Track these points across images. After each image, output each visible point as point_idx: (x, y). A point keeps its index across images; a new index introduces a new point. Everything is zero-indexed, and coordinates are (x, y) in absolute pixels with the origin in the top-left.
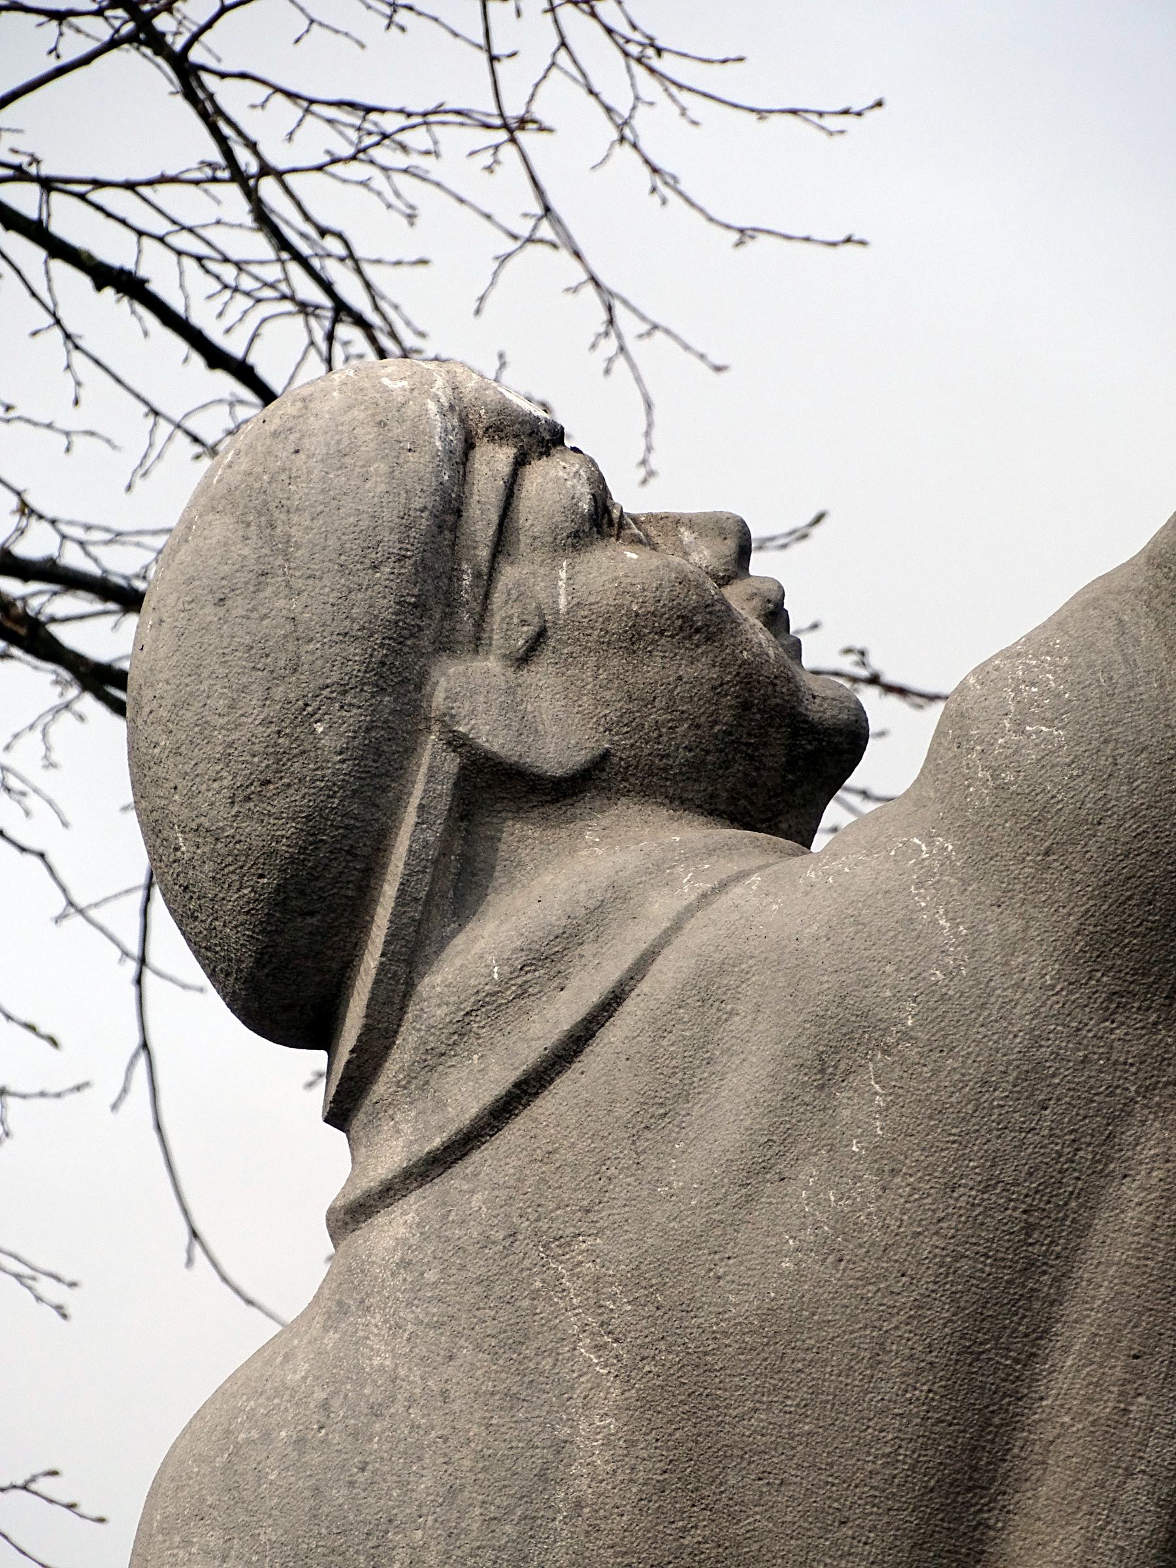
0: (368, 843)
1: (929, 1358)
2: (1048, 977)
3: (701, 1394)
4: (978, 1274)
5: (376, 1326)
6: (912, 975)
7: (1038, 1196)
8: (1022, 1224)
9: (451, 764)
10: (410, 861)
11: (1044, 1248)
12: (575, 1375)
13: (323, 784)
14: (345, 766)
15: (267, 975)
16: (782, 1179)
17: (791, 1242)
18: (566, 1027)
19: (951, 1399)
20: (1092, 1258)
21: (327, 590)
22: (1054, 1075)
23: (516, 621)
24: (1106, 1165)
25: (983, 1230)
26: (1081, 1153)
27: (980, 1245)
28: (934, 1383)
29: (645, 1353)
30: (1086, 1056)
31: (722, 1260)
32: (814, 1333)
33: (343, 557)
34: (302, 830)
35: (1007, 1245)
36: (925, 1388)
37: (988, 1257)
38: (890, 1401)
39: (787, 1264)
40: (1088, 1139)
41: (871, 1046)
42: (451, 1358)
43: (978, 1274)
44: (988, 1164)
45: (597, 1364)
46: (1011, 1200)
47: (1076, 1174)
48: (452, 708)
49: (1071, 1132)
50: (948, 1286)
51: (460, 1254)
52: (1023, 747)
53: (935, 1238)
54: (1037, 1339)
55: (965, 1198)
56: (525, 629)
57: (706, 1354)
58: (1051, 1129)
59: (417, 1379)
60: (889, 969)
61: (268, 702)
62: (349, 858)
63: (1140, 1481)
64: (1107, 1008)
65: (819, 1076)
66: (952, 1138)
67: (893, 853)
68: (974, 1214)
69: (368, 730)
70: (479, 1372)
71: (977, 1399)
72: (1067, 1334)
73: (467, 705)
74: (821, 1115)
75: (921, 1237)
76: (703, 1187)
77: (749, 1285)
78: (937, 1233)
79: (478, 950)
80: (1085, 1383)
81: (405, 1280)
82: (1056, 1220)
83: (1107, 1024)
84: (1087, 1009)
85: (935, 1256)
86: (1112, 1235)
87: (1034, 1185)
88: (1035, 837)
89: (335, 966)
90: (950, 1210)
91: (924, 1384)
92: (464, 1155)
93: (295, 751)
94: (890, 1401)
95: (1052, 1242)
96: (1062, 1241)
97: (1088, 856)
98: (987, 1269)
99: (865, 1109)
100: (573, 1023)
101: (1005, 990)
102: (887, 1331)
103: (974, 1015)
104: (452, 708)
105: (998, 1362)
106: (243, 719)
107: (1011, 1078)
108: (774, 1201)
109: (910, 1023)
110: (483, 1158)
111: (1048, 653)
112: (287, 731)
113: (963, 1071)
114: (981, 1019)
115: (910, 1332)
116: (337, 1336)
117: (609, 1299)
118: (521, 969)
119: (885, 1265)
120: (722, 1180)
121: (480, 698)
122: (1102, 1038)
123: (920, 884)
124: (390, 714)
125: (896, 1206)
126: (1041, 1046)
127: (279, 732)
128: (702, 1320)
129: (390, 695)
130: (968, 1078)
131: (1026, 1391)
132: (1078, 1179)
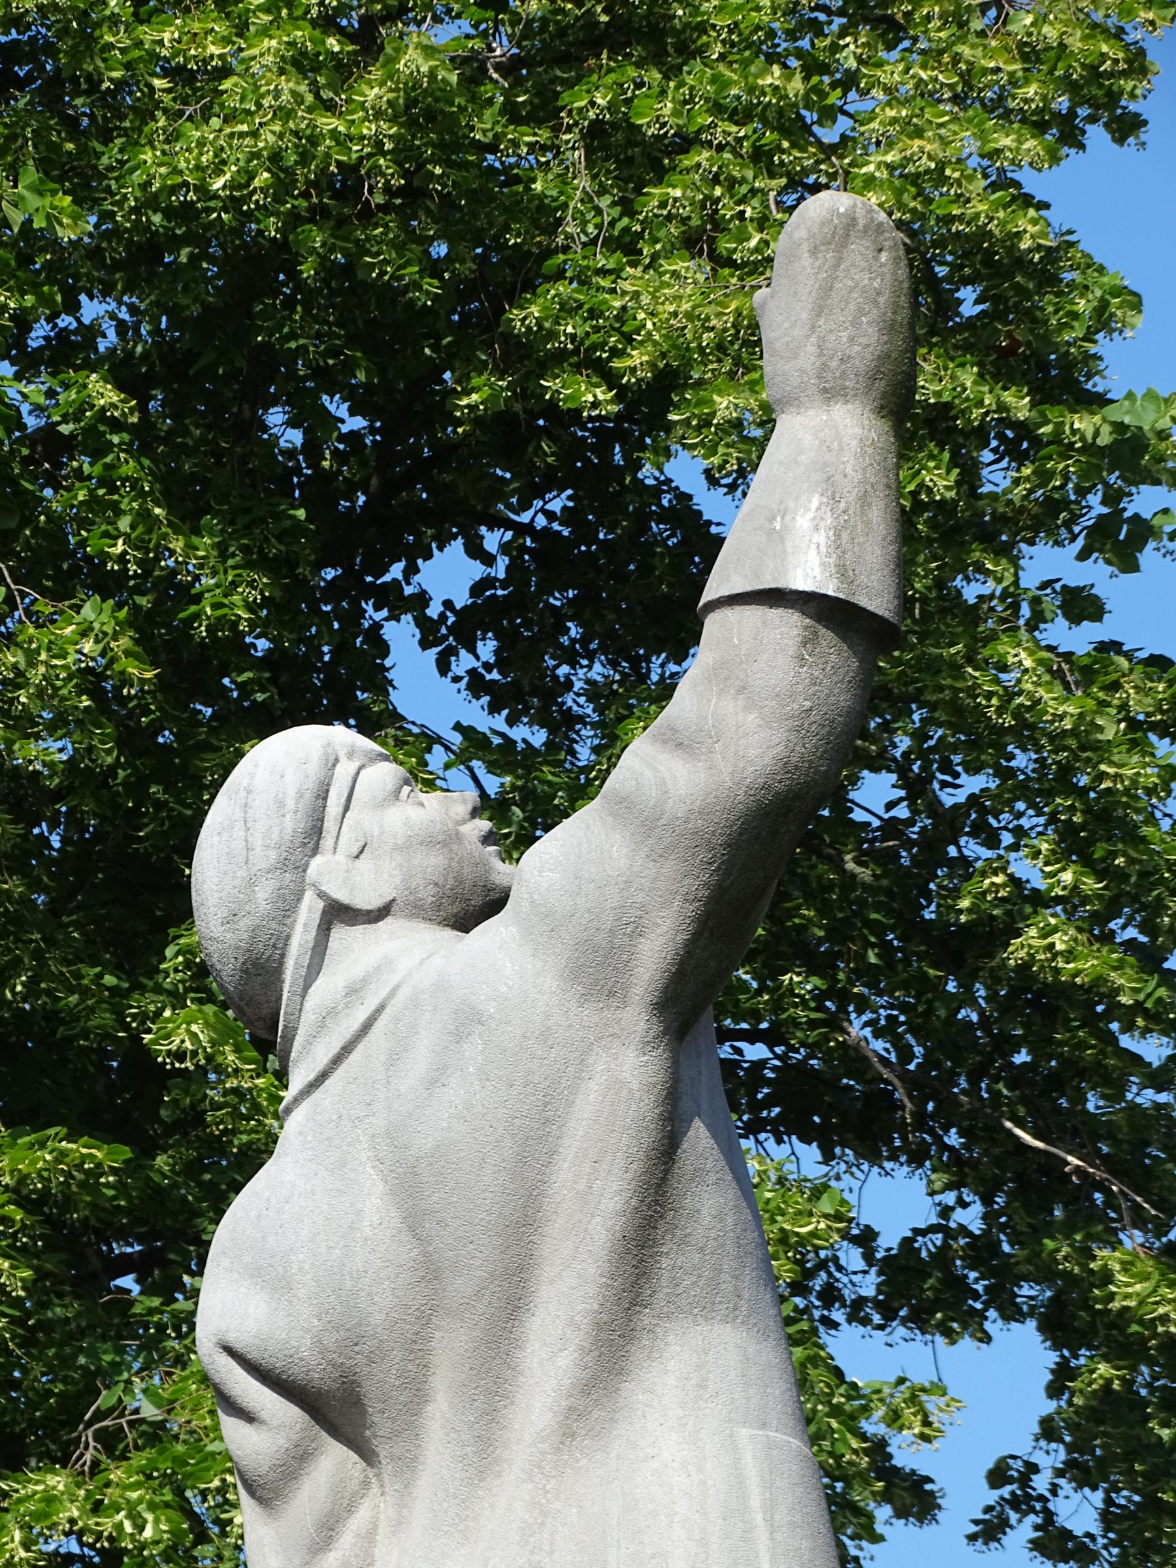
9: (320, 905)
63: (598, 1219)
99: (473, 1050)
121: (332, 873)
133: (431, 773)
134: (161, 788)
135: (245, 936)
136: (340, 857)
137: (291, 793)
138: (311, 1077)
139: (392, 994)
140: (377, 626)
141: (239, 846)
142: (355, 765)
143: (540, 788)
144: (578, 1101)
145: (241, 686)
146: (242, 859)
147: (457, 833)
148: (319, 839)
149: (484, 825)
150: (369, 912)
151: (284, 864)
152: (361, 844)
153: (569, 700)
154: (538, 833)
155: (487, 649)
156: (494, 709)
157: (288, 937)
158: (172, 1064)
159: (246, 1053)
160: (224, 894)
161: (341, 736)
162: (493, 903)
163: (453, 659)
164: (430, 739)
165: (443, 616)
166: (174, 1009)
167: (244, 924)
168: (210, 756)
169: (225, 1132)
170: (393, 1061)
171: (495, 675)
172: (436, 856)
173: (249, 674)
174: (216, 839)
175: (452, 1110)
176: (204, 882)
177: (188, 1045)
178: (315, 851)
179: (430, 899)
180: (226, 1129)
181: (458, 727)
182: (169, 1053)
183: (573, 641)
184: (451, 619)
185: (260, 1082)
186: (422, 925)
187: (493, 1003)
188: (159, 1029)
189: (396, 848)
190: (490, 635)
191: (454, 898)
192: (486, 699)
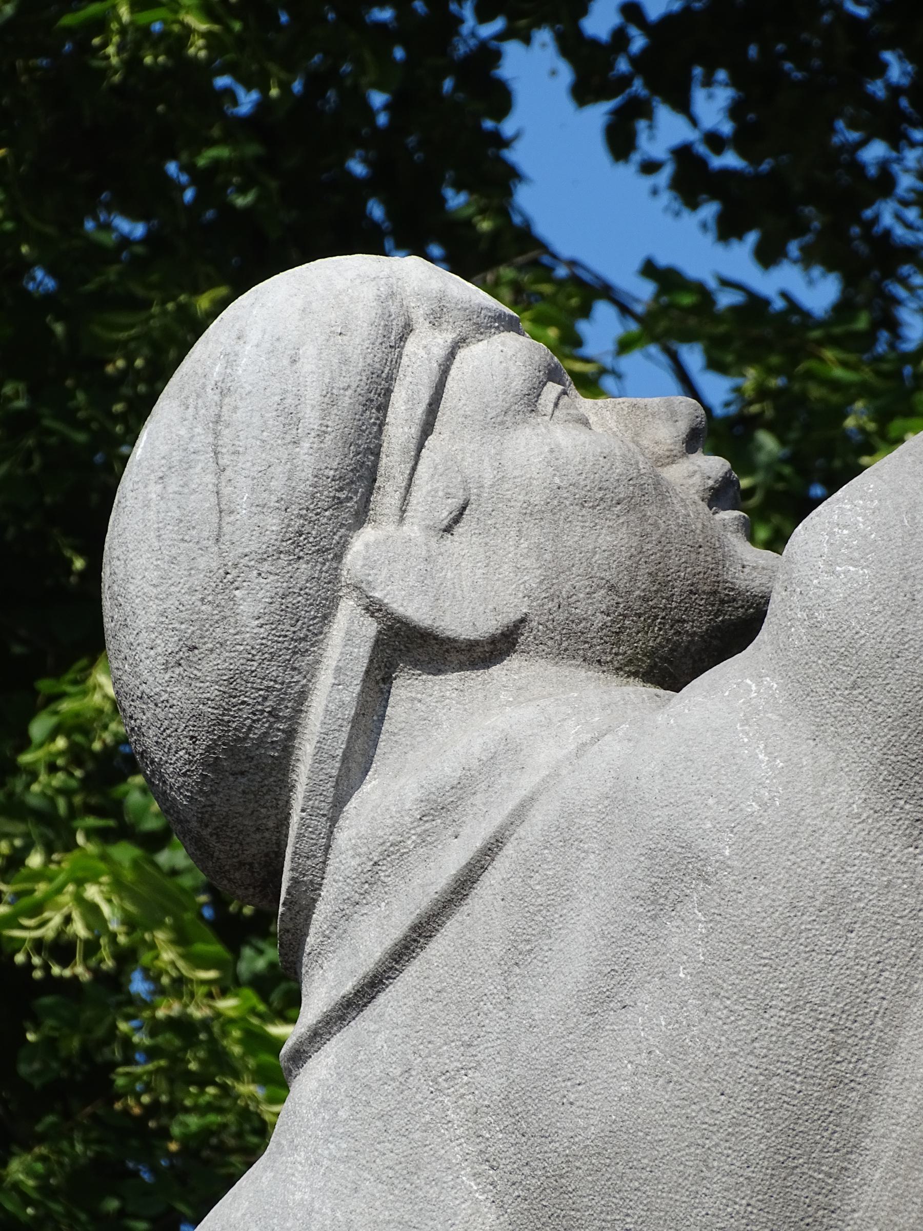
0: (290, 705)
1: (748, 1173)
2: (855, 806)
3: (558, 1216)
4: (789, 1091)
5: (301, 1164)
6: (731, 807)
7: (844, 1016)
8: (830, 1043)
9: (370, 628)
10: (327, 721)
11: (851, 1066)
12: (457, 1202)
13: (242, 648)
14: (262, 630)
15: (211, 835)
16: (624, 1007)
17: (629, 1066)
18: (454, 872)
19: (768, 1212)
20: (898, 1075)
21: (249, 464)
22: (859, 900)
23: (441, 494)
24: (910, 985)
25: (792, 1049)
26: (886, 974)
27: (790, 1063)
28: (752, 1198)
29: (514, 1178)
30: (889, 881)
31: (573, 1086)
32: (648, 1153)
33: (265, 434)
34: (224, 692)
35: (816, 1063)
36: (744, 1202)
37: (798, 1075)
38: (713, 1215)
39: (626, 1088)
40: (893, 961)
41: (694, 876)
42: (356, 1190)
43: (789, 1091)
44: (796, 986)
45: (476, 1191)
46: (819, 1020)
47: (881, 994)
48: (369, 575)
49: (876, 954)
50: (761, 1104)
51: (366, 1091)
52: (833, 586)
53: (750, 1057)
54: (848, 1153)
55: (776, 1018)
56: (450, 501)
57: (561, 1176)
58: (856, 952)
59: (329, 1212)
60: (711, 801)
61: (193, 572)
62: (272, 720)
64: (911, 835)
65: (651, 908)
66: (763, 961)
67: (727, 694)
68: (784, 1034)
69: (284, 597)
70: (378, 1203)
71: (792, 1212)
72: (875, 1148)
73: (384, 572)
74: (654, 944)
75: (737, 1057)
76: (559, 1017)
77: (594, 1109)
78: (751, 1053)
79: (383, 799)
80: (891, 1195)
81: (324, 1119)
82: (862, 1038)
83: (911, 849)
84: (892, 836)
85: (750, 1075)
86: (916, 1053)
87: (841, 1005)
88: (843, 672)
89: (271, 824)
90: (763, 1031)
91: (743, 1198)
92: (373, 998)
93: (217, 617)
94: (713, 1215)
95: (859, 1060)
96: (868, 1059)
97: (888, 688)
98: (797, 1086)
99: (686, 936)
100: (459, 867)
101: (815, 818)
102: (709, 1148)
103: (785, 844)
104: (369, 575)
105: (811, 1176)
106: (173, 589)
107: (817, 903)
108: (616, 1028)
109: (727, 853)
110: (386, 1001)
111: (861, 498)
112: (210, 598)
113: (774, 897)
114: (791, 847)
115: (730, 1148)
116: (272, 1174)
117: (485, 1128)
118: (420, 819)
119: (706, 1085)
120: (573, 1010)
121: (396, 561)
122: (905, 863)
123: (746, 722)
124: (307, 581)
125: (715, 1028)
126: (847, 872)
127: (202, 599)
128: (557, 1145)
129: (308, 562)
130: (778, 903)
131: (839, 1204)
132: (883, 998)
133: (587, 360)
134: (21, 387)
135: (214, 692)
136: (413, 530)
137: (313, 395)
138: (348, 987)
139: (519, 815)
140: (488, 55)
141: (201, 504)
142: (446, 337)
143: (815, 392)
144: (903, 1042)
145: (199, 177)
146: (207, 531)
147: (658, 482)
148: (370, 491)
149: (715, 466)
150: (472, 645)
151: (295, 544)
152: (455, 503)
153: (886, 214)
154: (817, 491)
155: (713, 105)
156: (728, 229)
157: (303, 696)
158: (46, 968)
159: (200, 947)
160: (171, 603)
161: (416, 277)
162: (734, 626)
163: (642, 125)
164: (590, 291)
165: (620, 38)
166: (49, 850)
167: (212, 666)
168: (122, 318)
169: (153, 1109)
170: (520, 953)
171: (730, 160)
172: (613, 530)
173: (222, 152)
174: (155, 489)
175: (643, 1059)
176: (128, 579)
177: (79, 928)
178: (361, 517)
179: (599, 620)
180: (156, 1103)
181: (649, 269)
182: (39, 945)
183: (895, 91)
184: (638, 42)
185: (228, 1005)
186: (582, 674)
187: (728, 836)
188: (18, 895)
189: (528, 512)
190: (721, 75)
191: (649, 618)
192: (710, 210)
